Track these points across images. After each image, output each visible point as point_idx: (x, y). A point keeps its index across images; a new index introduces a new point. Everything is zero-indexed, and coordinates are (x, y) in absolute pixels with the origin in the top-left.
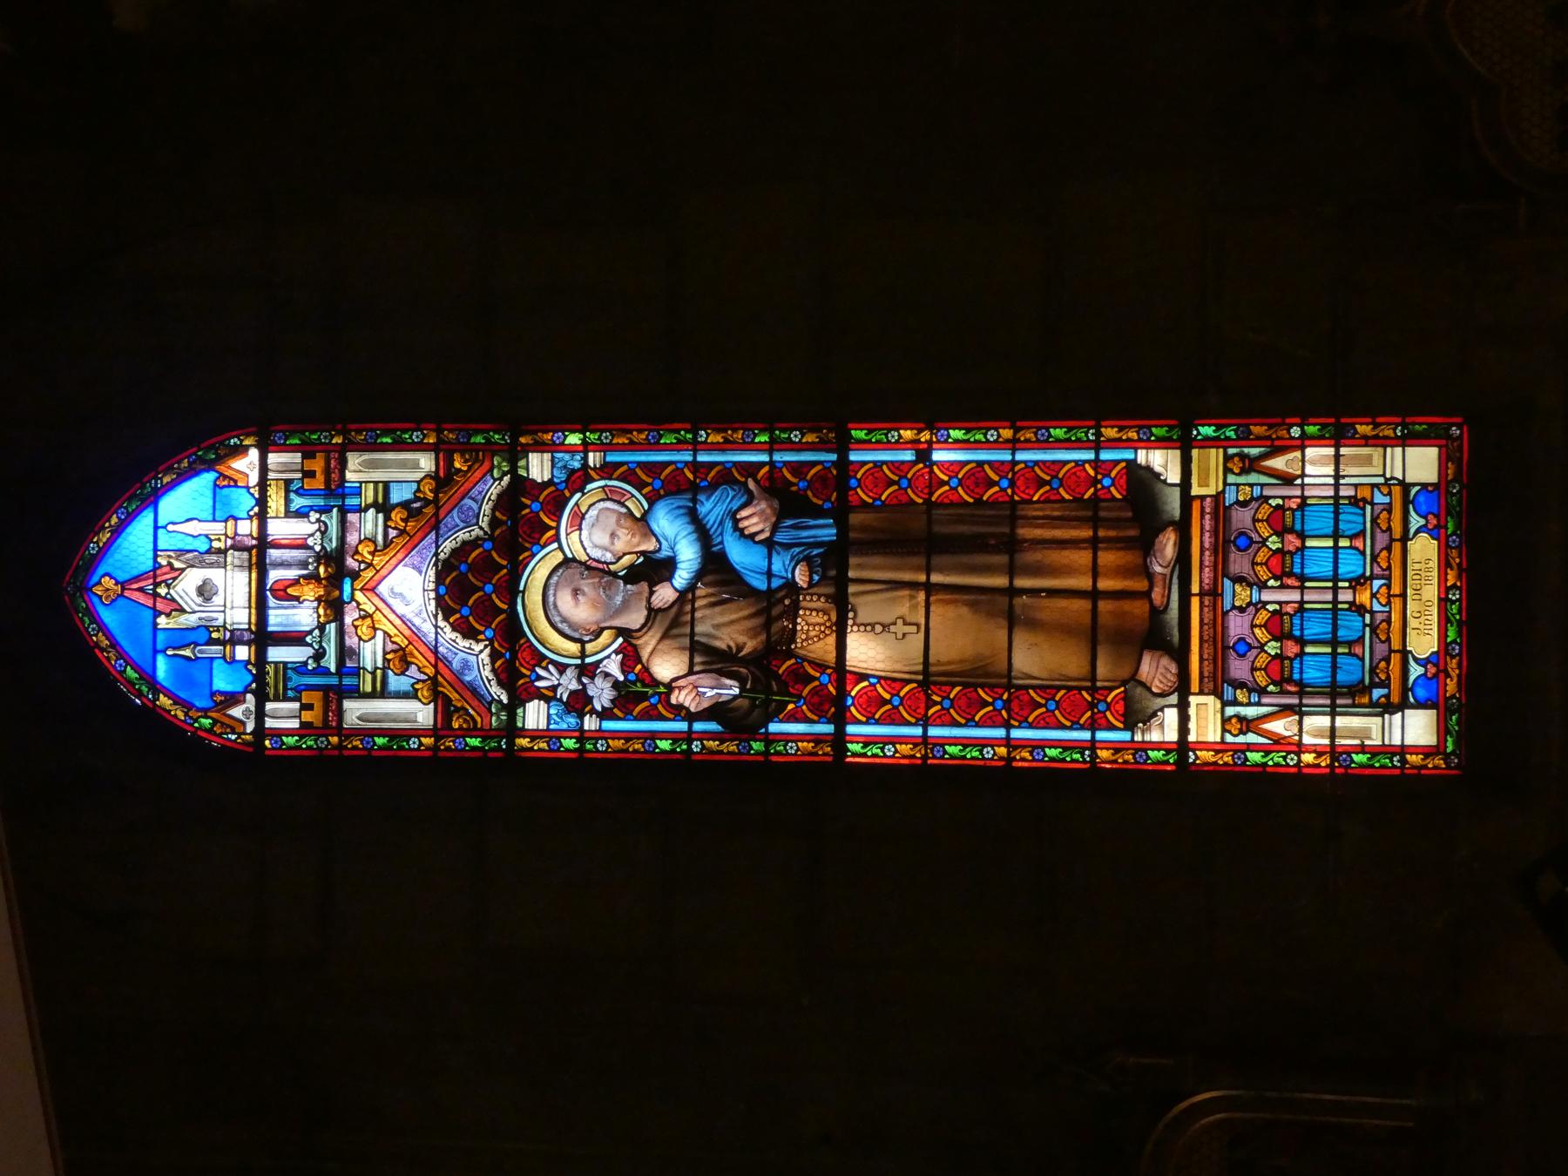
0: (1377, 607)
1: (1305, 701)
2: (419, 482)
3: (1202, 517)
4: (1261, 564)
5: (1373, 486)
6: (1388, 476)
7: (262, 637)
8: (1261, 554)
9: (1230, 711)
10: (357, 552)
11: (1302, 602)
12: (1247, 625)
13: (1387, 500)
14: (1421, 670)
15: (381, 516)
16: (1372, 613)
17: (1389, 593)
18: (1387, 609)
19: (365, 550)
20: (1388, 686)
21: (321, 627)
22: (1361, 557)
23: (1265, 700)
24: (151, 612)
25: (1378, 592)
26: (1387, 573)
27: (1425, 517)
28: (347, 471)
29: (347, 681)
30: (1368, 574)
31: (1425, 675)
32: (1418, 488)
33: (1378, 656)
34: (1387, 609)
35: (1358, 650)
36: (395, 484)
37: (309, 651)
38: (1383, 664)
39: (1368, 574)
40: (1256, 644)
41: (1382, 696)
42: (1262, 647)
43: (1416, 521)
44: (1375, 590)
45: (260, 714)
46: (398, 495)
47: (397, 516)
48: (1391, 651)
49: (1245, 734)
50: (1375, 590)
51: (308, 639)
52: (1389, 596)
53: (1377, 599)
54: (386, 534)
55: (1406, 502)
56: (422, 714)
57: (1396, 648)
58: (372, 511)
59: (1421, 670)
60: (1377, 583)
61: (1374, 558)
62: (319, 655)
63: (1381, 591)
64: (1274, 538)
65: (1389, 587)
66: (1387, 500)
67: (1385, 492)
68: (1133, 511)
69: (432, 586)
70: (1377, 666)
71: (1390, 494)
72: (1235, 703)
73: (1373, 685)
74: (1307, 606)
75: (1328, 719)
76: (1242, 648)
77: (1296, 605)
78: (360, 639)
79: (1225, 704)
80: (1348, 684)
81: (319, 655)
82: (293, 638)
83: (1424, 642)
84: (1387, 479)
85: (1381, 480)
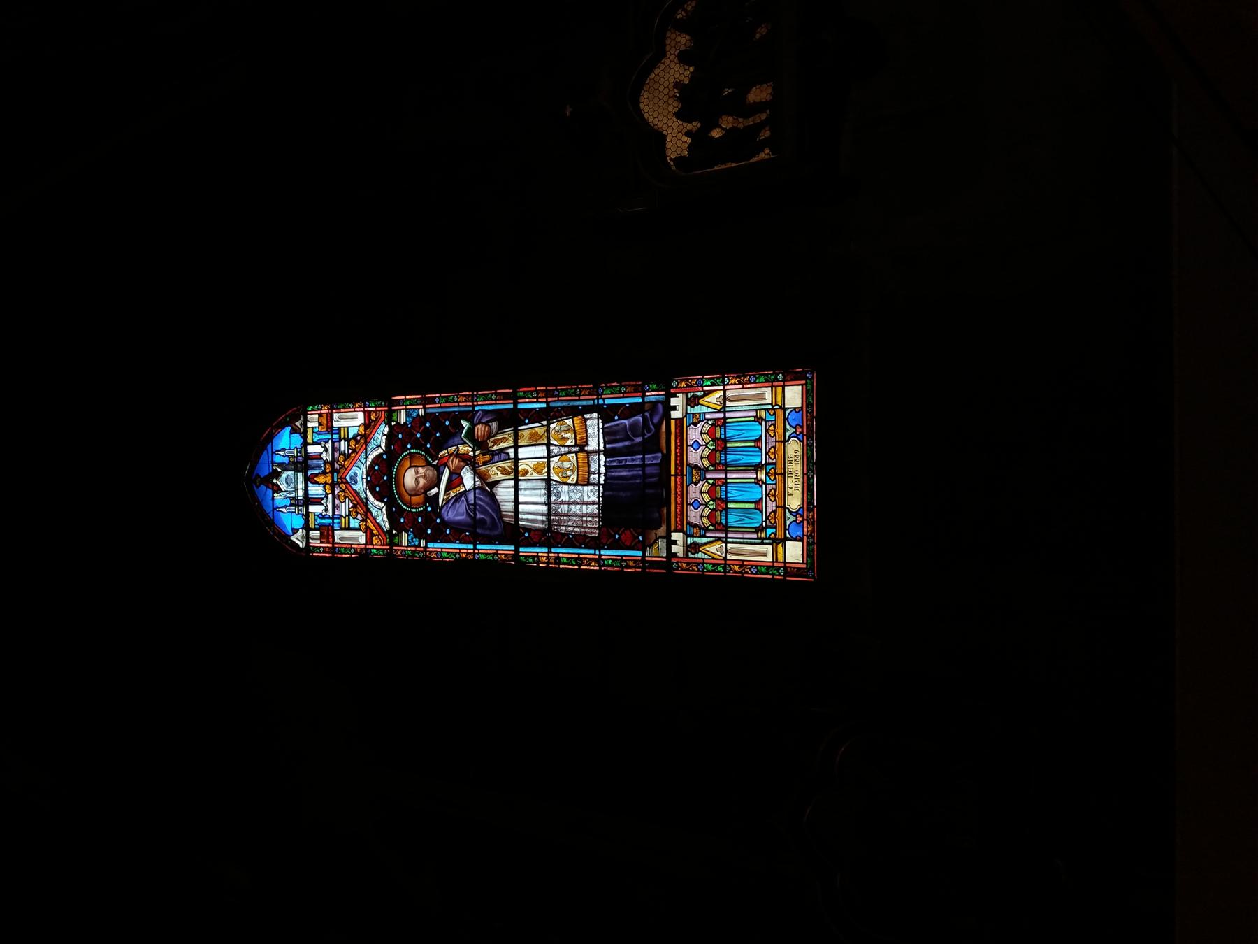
0: (769, 481)
1: (729, 535)
2: (359, 426)
3: (676, 497)
4: (705, 433)
5: (766, 410)
6: (774, 404)
8: (705, 452)
10: (338, 461)
11: (725, 418)
12: (699, 491)
14: (793, 518)
15: (346, 443)
16: (766, 484)
18: (774, 482)
19: (341, 459)
20: (775, 528)
23: (708, 535)
25: (769, 472)
27: (795, 428)
30: (764, 462)
31: (795, 521)
32: (789, 410)
33: (770, 510)
34: (774, 461)
37: (323, 507)
38: (772, 450)
39: (764, 462)
40: (704, 444)
41: (772, 533)
42: (706, 505)
43: (790, 431)
44: (768, 471)
46: (352, 432)
47: (352, 443)
48: (777, 507)
50: (768, 471)
51: (323, 502)
52: (776, 474)
54: (348, 451)
55: (785, 419)
56: (361, 538)
58: (343, 441)
59: (793, 518)
60: (769, 467)
62: (326, 510)
63: (770, 428)
64: (712, 502)
67: (772, 413)
69: (364, 477)
70: (769, 451)
71: (775, 413)
72: (692, 536)
73: (767, 527)
74: (728, 420)
76: (696, 505)
77: (723, 480)
78: (340, 502)
79: (688, 536)
80: (754, 464)
81: (326, 510)
83: (795, 501)
84: (773, 406)
85: (770, 407)
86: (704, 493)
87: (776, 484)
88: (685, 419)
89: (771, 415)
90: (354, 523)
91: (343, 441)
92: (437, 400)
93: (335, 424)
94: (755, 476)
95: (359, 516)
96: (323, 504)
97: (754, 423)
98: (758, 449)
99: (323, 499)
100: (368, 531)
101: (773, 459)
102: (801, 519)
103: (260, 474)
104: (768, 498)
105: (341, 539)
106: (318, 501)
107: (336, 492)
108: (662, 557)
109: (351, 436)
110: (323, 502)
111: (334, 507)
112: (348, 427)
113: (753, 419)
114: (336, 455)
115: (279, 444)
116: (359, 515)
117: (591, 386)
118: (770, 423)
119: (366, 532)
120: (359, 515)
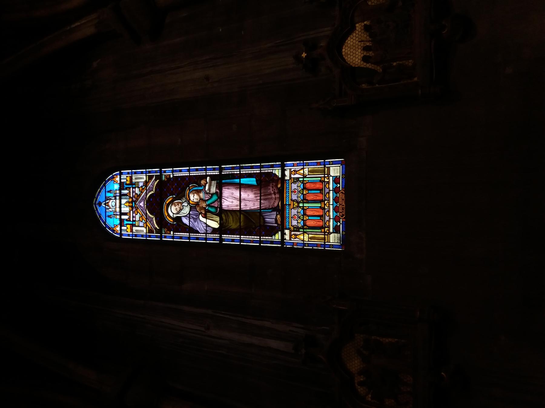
7: (121, 214)
9: (292, 233)
13: (328, 180)
15: (138, 189)
17: (329, 204)
18: (328, 208)
21: (130, 212)
22: (322, 195)
24: (105, 208)
26: (328, 199)
28: (361, 66)
29: (134, 223)
34: (328, 208)
35: (322, 218)
36: (141, 183)
45: (121, 230)
49: (296, 238)
51: (128, 214)
53: (326, 206)
57: (320, 231)
58: (137, 188)
61: (325, 196)
65: (329, 203)
66: (328, 180)
68: (220, 224)
75: (332, 218)
82: (125, 214)
86: (298, 197)
87: (329, 209)
88: (290, 180)
89: (328, 189)
90: (141, 224)
91: (137, 188)
92: (134, 235)
93: (133, 181)
94: (320, 205)
95: (143, 221)
96: (128, 215)
97: (320, 183)
98: (321, 221)
99: (128, 213)
100: (147, 227)
101: (328, 207)
102: (339, 224)
103: (101, 201)
104: (326, 197)
105: (136, 231)
106: (125, 214)
107: (134, 210)
108: (286, 202)
109: (140, 187)
110: (128, 214)
111: (133, 217)
112: (139, 182)
113: (319, 207)
114: (134, 194)
115: (109, 187)
116: (143, 220)
117: (223, 229)
118: (326, 210)
119: (146, 228)
120: (143, 220)
